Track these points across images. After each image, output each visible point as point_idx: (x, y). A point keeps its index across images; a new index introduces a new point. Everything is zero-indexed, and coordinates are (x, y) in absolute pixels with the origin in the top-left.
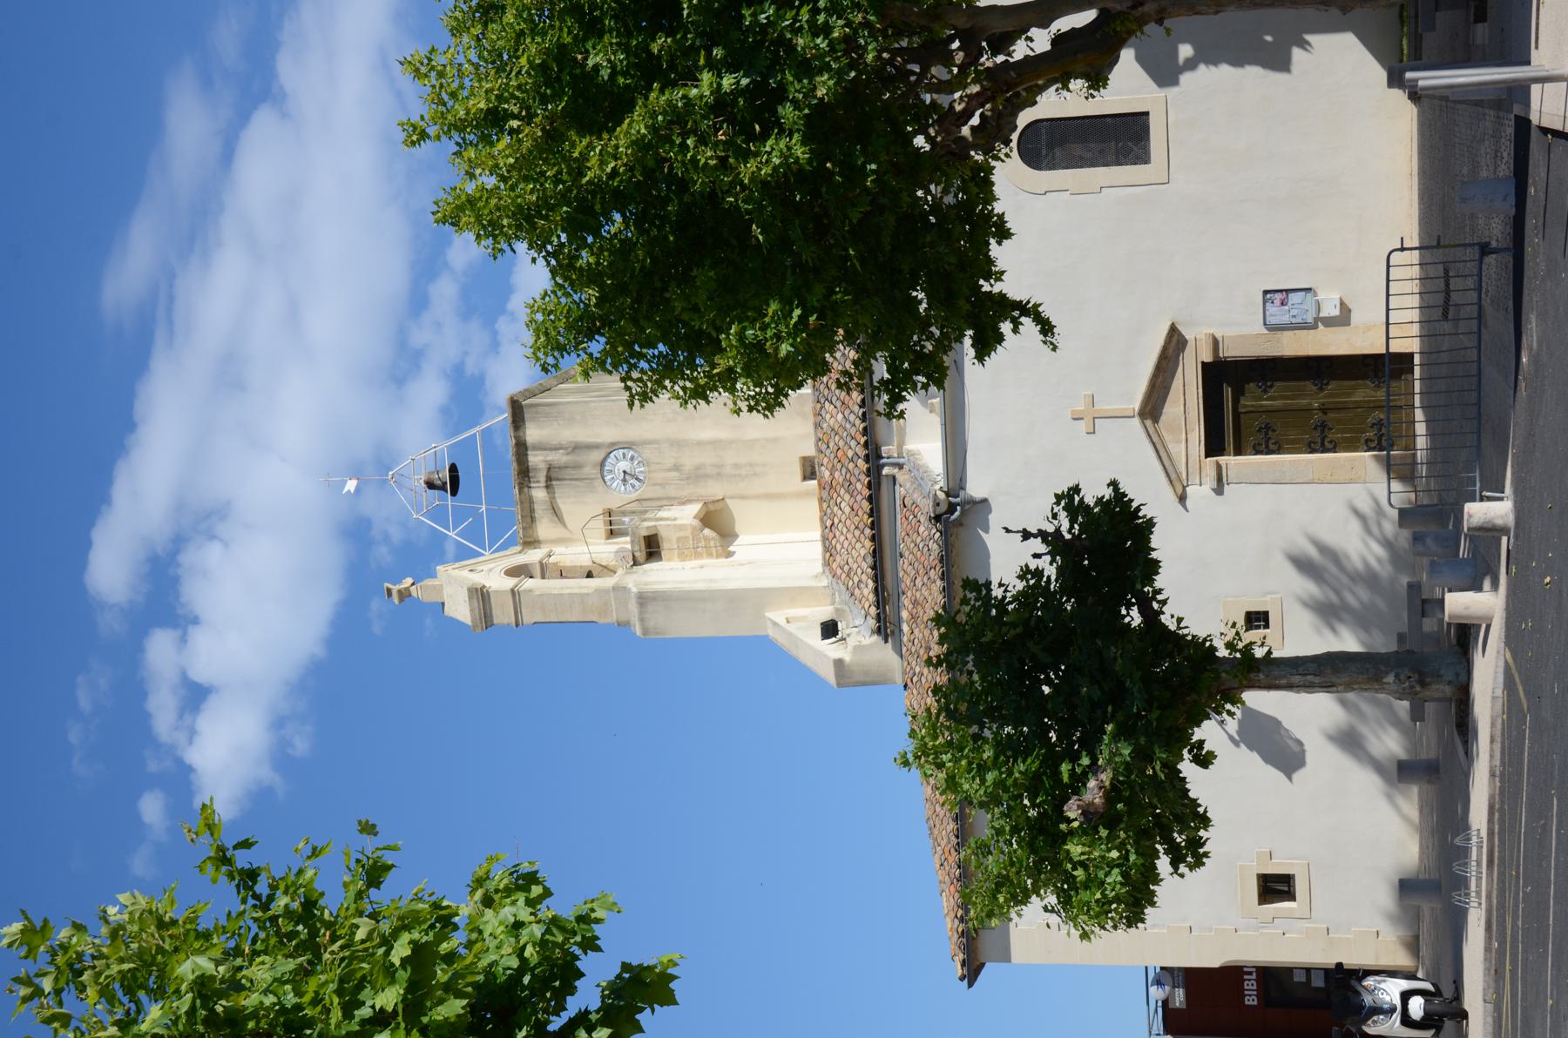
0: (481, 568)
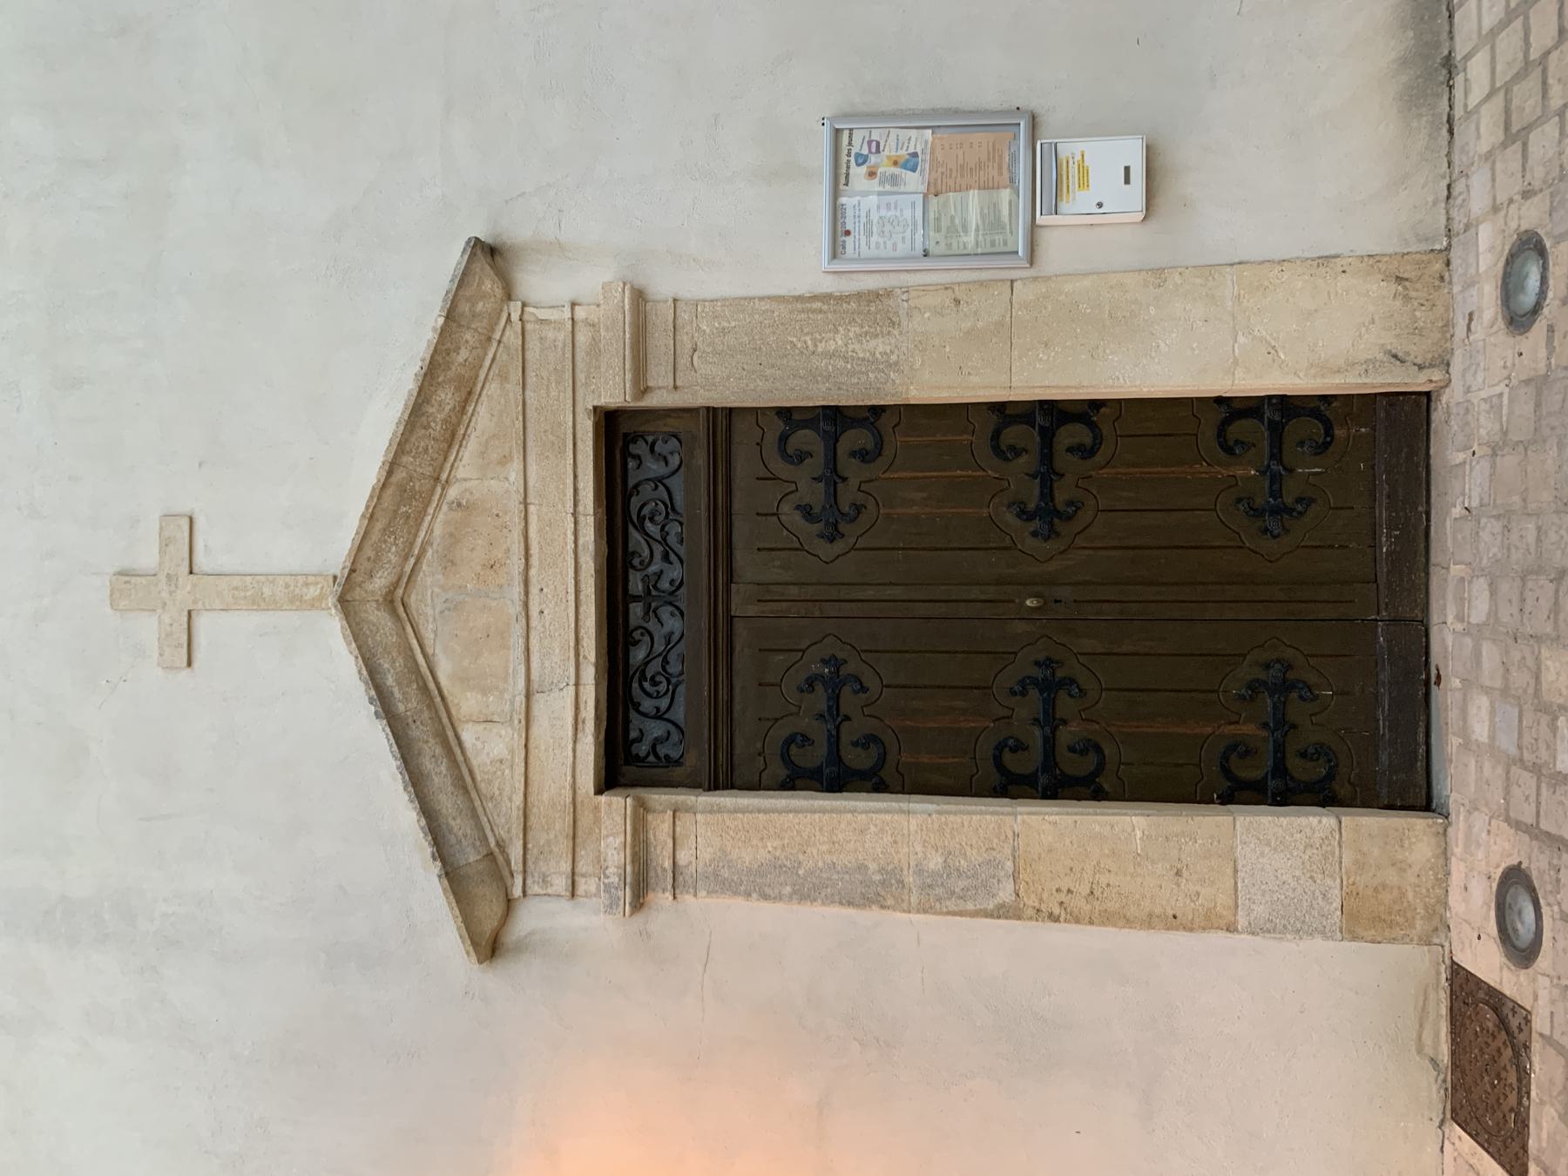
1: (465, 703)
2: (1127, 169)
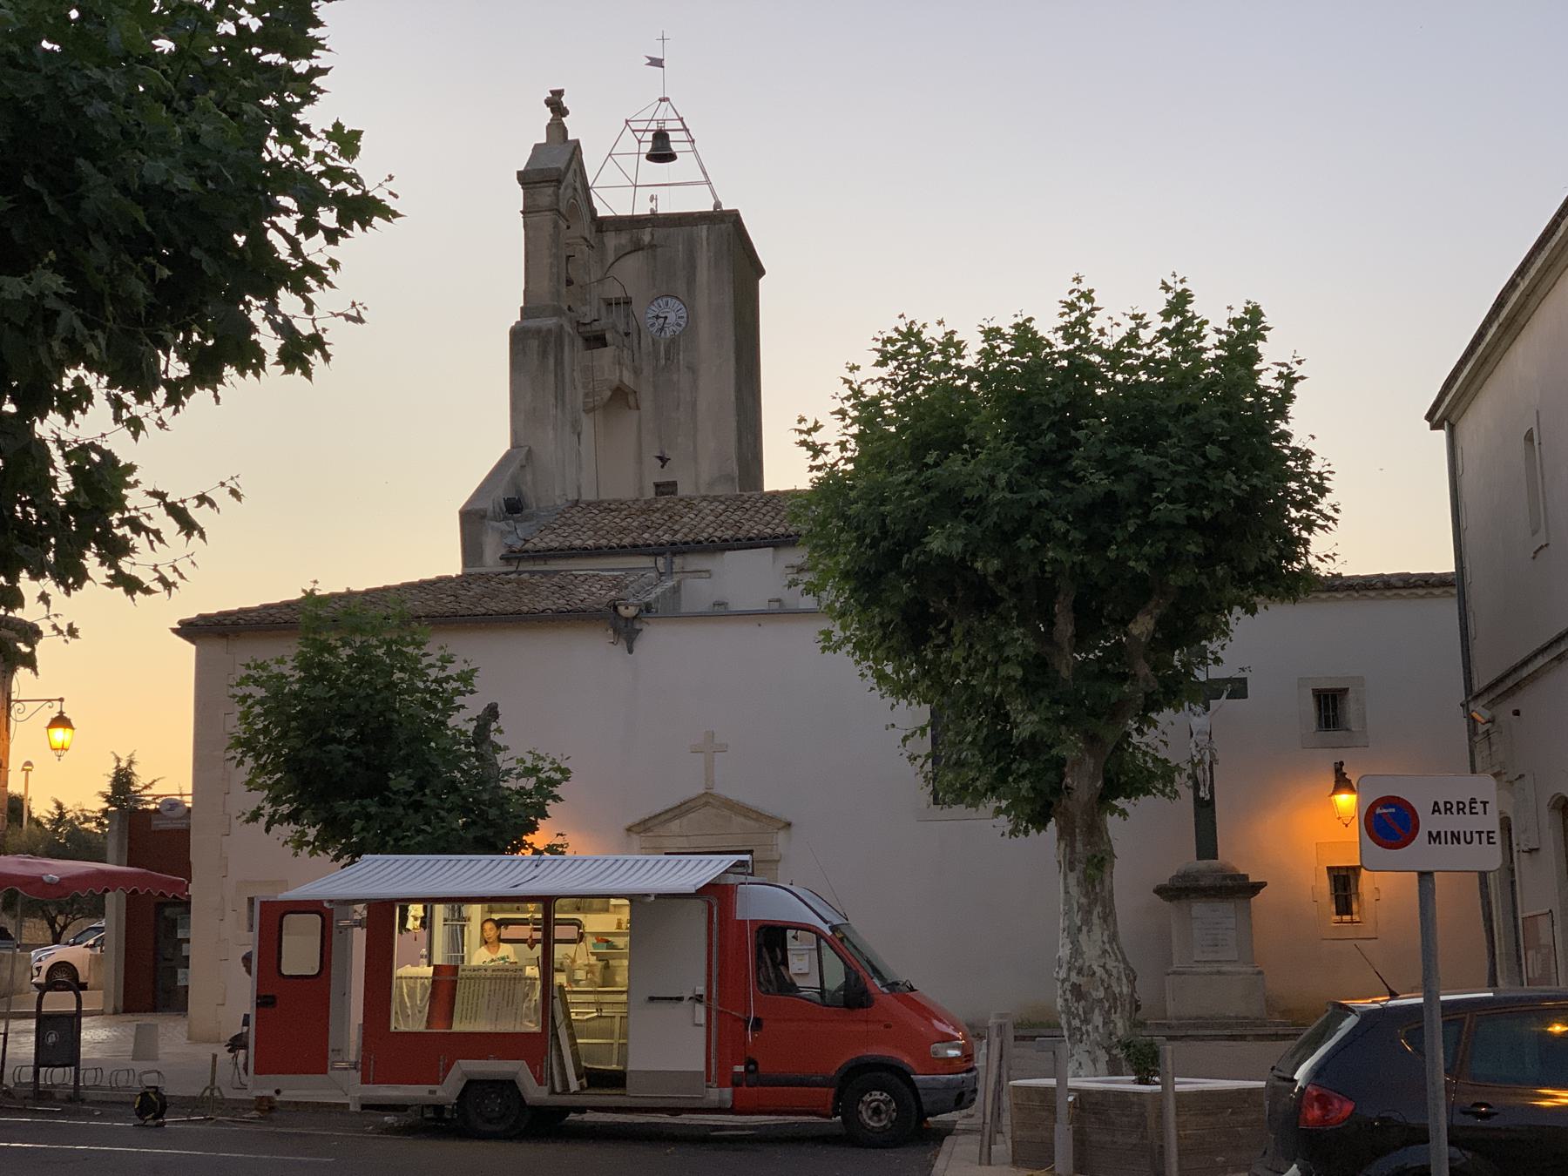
0: (578, 181)
1: (685, 820)
2: (396, 196)
